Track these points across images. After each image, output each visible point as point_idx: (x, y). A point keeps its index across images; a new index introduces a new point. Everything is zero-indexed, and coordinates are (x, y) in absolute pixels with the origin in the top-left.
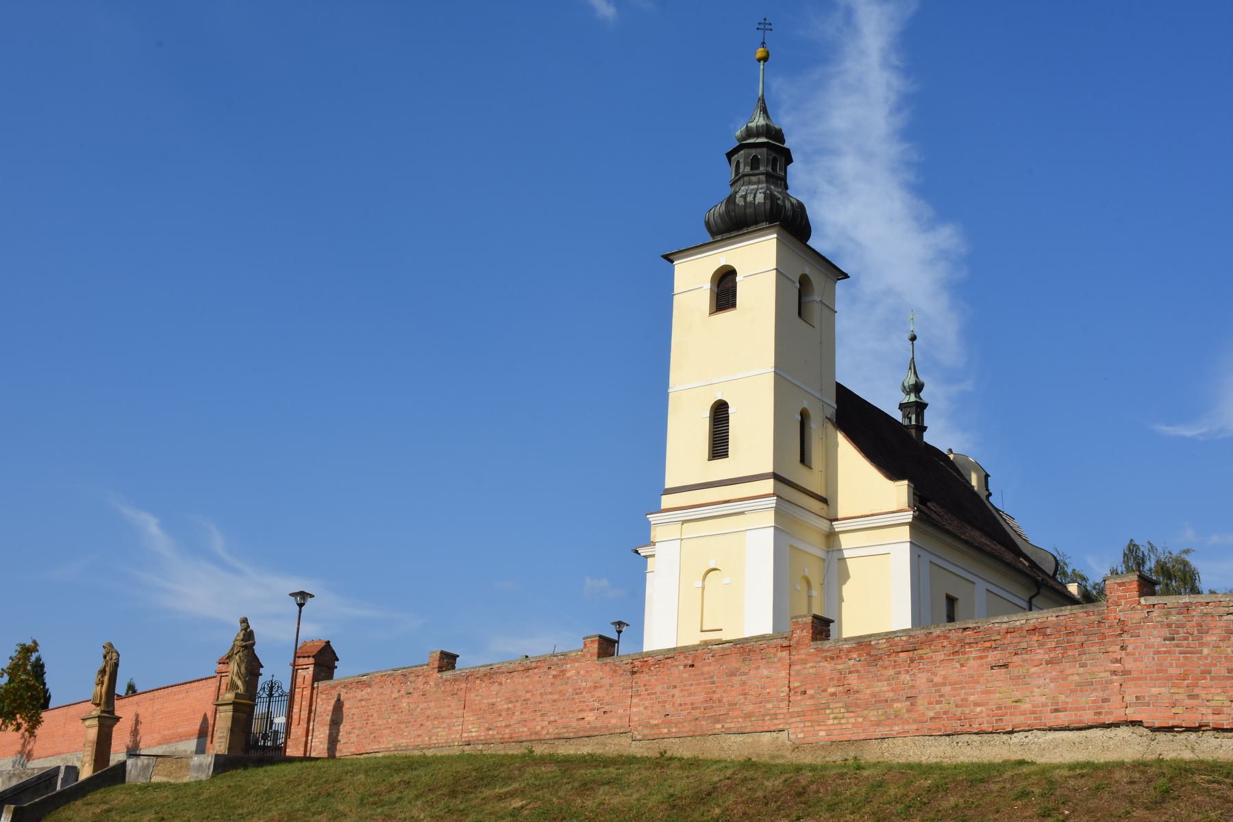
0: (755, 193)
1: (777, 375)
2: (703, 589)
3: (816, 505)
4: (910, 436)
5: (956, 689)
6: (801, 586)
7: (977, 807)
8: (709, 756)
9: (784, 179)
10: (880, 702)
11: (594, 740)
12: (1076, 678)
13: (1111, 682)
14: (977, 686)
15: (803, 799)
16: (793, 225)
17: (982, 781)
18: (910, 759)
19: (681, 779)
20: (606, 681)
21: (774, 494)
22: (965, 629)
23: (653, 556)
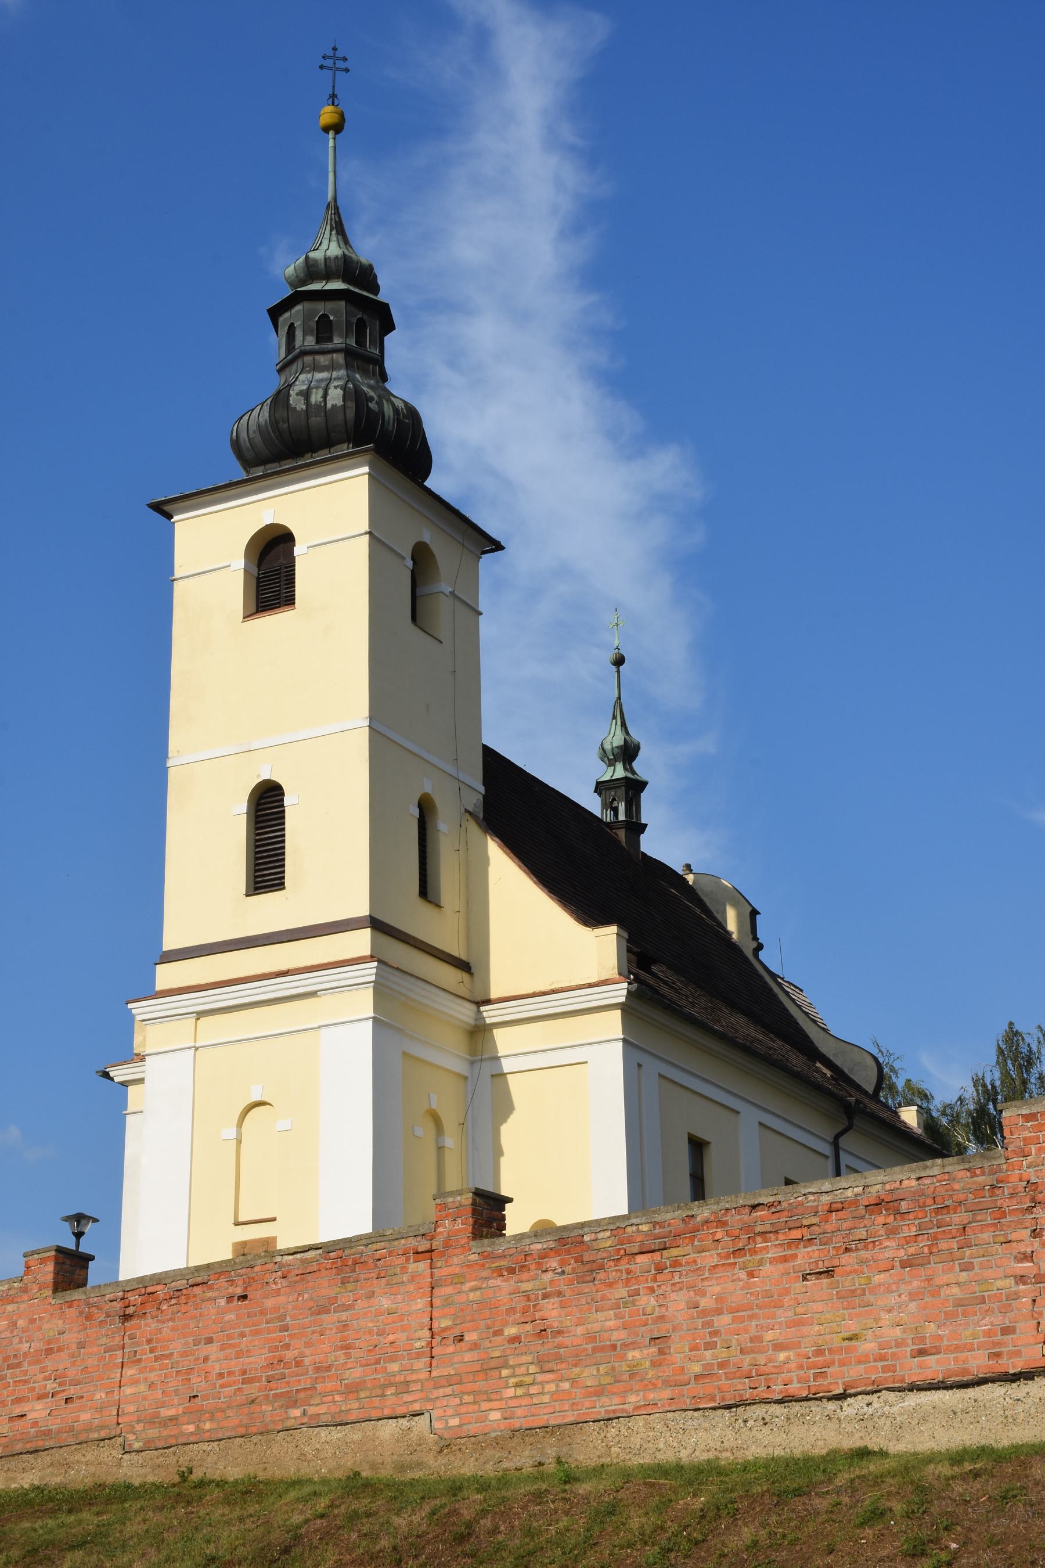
0: (327, 388)
1: (374, 732)
2: (239, 1141)
3: (449, 976)
4: (616, 842)
5: (742, 1320)
6: (425, 1130)
7: (792, 1543)
8: (279, 1474)
9: (378, 362)
10: (602, 1349)
11: (45, 1458)
12: (955, 1290)
13: (1017, 1296)
14: (779, 1312)
15: (468, 1548)
16: (398, 449)
17: (798, 1492)
18: (660, 1456)
19: (228, 1523)
20: (71, 1338)
21: (372, 958)
22: (754, 1207)
23: (141, 1081)
